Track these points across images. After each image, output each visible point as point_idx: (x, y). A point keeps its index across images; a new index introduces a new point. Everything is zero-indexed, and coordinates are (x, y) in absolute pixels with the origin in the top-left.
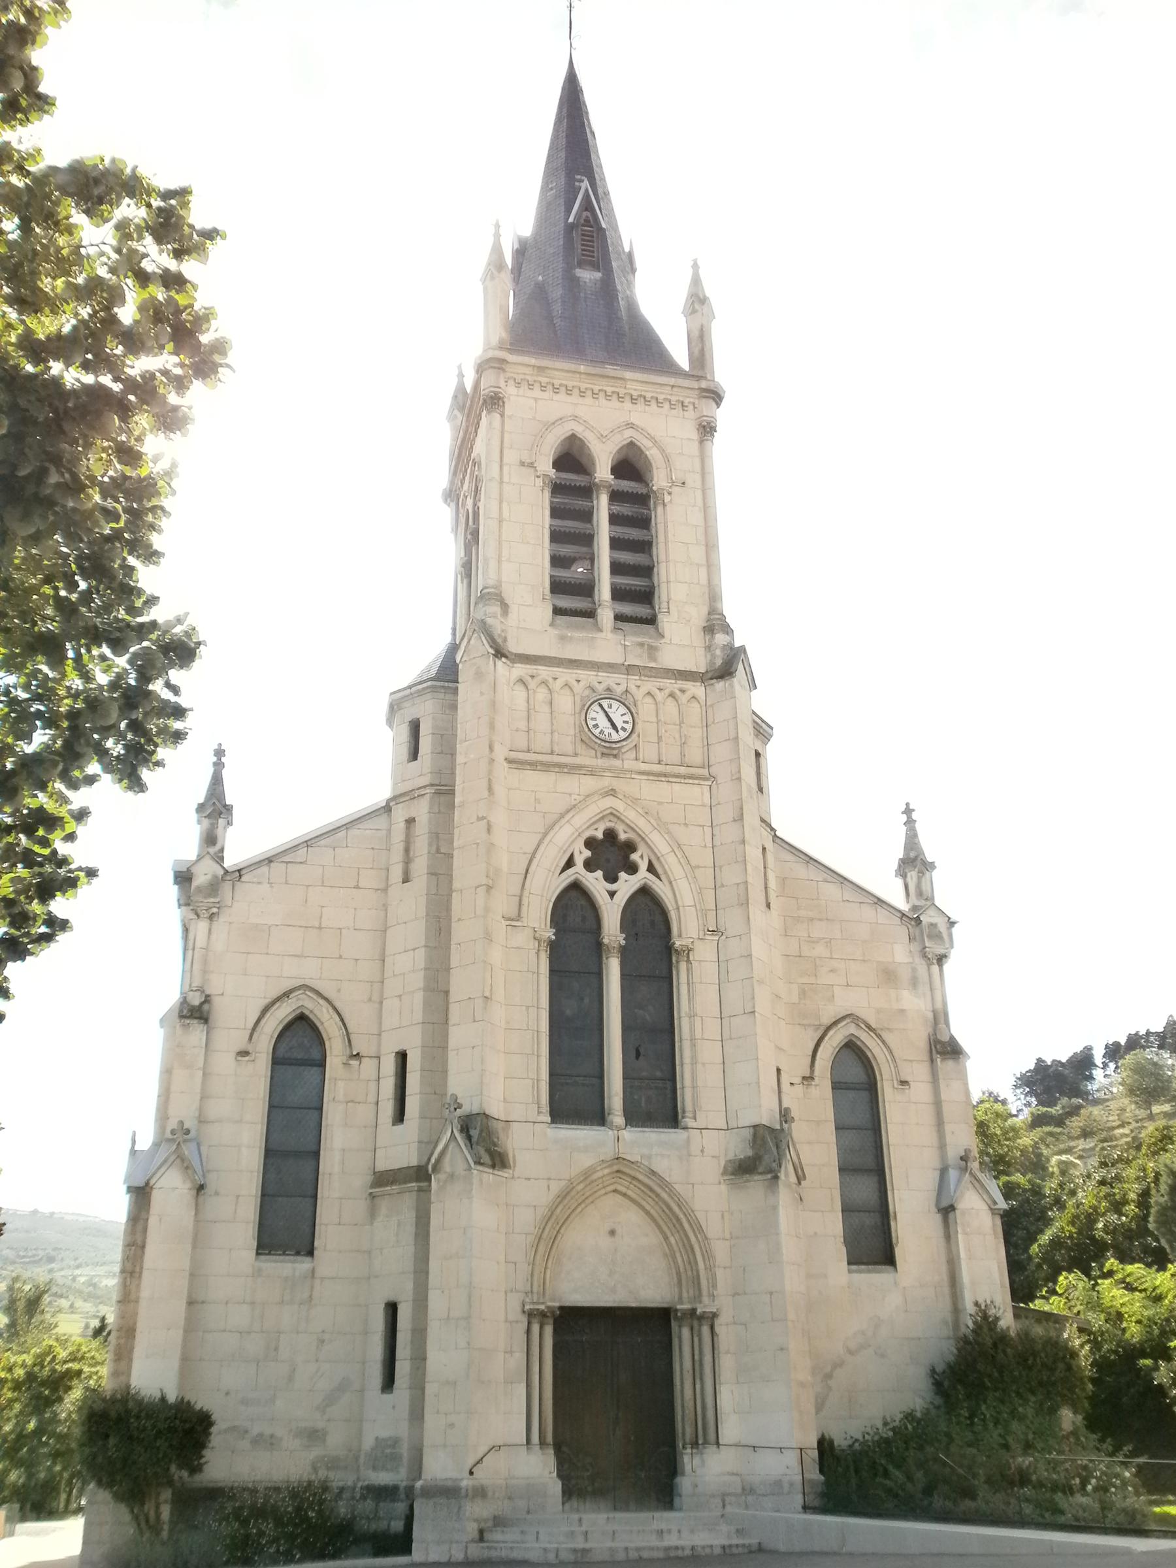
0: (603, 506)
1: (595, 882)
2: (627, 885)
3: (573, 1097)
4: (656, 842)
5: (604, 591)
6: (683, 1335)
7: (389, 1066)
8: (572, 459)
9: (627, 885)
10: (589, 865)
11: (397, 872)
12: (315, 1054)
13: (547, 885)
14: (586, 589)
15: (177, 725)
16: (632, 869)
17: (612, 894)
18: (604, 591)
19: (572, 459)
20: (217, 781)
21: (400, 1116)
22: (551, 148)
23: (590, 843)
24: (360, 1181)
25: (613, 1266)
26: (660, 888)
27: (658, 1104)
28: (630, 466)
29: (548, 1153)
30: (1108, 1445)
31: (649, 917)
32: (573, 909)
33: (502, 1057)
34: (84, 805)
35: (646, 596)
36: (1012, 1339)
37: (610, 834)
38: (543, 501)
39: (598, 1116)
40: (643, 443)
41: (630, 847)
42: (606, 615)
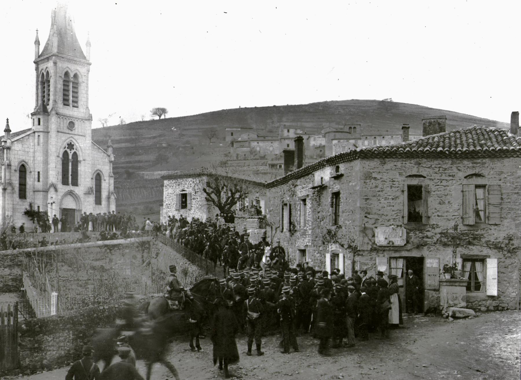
1: (68, 151)
2: (73, 151)
3: (65, 182)
4: (77, 145)
7: (37, 174)
8: (67, 74)
9: (73, 151)
10: (68, 148)
11: (36, 143)
12: (24, 170)
13: (62, 151)
14: (68, 100)
15: (72, 75)
16: (73, 149)
20: (8, 125)
22: (230, 110)
27: (75, 183)
28: (76, 76)
29: (63, 189)
31: (75, 154)
32: (66, 154)
33: (54, 175)
35: (76, 102)
37: (71, 143)
39: (68, 184)
40: (78, 73)
41: (73, 145)
42: (71, 105)
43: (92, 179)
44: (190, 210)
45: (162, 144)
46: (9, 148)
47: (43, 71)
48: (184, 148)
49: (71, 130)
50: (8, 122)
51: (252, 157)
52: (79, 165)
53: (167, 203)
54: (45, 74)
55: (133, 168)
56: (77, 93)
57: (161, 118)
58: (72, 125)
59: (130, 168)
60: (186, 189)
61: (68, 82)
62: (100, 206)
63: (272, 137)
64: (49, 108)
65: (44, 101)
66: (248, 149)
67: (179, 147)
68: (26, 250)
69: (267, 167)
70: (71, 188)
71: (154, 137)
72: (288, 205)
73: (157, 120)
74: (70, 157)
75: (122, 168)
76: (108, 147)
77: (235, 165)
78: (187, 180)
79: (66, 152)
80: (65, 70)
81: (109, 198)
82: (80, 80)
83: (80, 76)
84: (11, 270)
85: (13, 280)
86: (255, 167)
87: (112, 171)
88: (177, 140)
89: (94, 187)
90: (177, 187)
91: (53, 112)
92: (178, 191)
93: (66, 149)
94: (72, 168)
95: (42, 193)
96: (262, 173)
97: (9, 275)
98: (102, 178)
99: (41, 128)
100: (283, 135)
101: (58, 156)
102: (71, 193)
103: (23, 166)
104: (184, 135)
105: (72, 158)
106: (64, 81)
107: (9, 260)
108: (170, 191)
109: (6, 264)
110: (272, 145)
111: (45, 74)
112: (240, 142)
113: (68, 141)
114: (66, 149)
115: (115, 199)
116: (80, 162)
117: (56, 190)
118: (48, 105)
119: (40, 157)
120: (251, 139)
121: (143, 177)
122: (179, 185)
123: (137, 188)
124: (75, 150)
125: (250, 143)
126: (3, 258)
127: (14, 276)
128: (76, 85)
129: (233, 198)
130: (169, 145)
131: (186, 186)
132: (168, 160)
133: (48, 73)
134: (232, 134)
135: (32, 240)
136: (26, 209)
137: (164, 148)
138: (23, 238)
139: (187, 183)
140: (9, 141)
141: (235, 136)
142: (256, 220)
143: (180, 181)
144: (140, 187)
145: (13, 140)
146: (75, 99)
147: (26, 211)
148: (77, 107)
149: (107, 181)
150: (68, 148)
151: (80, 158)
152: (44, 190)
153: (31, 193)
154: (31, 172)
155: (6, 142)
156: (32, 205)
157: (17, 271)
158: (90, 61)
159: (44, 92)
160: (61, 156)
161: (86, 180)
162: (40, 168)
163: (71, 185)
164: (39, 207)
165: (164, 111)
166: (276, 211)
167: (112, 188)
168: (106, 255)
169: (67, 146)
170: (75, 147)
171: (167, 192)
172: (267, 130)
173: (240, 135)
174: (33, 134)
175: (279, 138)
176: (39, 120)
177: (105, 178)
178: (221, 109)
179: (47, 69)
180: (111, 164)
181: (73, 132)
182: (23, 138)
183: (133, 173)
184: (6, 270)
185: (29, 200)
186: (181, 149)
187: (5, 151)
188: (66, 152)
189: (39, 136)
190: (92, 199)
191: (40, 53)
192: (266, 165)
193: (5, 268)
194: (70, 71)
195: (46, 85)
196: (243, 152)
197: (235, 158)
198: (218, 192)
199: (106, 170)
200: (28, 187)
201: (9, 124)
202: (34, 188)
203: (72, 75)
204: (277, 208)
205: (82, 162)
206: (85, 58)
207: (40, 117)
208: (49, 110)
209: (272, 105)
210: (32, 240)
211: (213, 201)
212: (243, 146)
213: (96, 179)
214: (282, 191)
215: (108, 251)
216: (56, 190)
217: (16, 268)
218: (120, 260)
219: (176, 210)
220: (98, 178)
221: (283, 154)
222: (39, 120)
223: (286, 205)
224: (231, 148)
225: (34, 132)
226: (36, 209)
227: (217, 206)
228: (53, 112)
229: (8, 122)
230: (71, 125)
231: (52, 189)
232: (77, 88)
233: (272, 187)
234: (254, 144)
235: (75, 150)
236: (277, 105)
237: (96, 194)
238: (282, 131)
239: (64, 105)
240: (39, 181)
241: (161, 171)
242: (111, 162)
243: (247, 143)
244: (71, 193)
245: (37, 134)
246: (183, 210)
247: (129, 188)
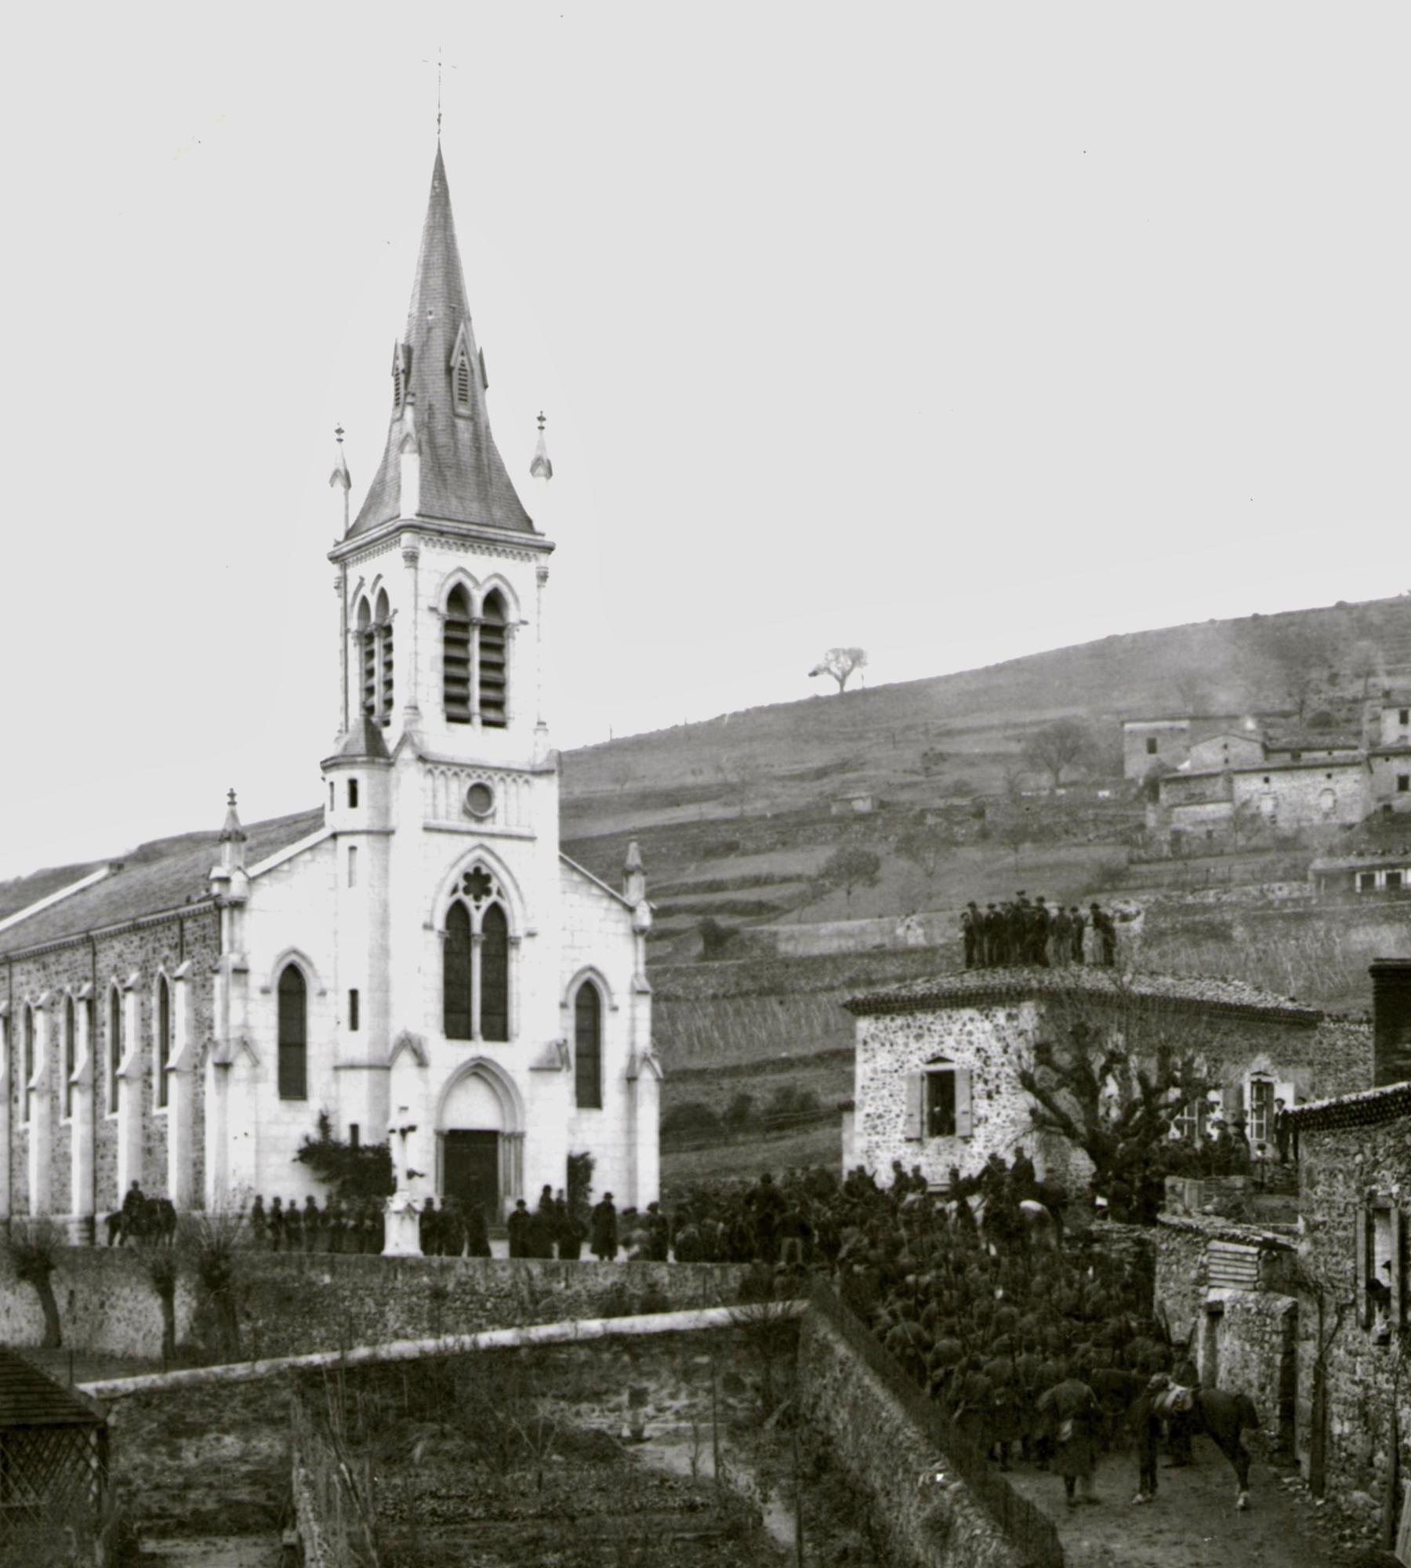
0: (475, 638)
1: (469, 901)
2: (486, 902)
3: (456, 1026)
4: (500, 878)
5: (475, 704)
6: (502, 1147)
9: (486, 902)
10: (466, 891)
13: (444, 903)
14: (463, 700)
15: (477, 598)
16: (488, 892)
17: (478, 908)
18: (475, 704)
19: (458, 597)
23: (467, 876)
25: (475, 1111)
26: (504, 904)
27: (498, 1029)
28: (494, 601)
30: (285, 1207)
31: (496, 915)
32: (458, 914)
33: (419, 1001)
34: (285, 946)
36: (502, 1212)
37: (477, 870)
38: (440, 665)
39: (467, 1036)
41: (487, 879)
42: (477, 720)
43: (563, 1006)
44: (967, 1139)
45: (850, 801)
46: (238, 905)
47: (365, 591)
48: (946, 813)
49: (480, 820)
50: (232, 803)
51: (1242, 842)
52: (513, 954)
53: (867, 1110)
54: (373, 602)
55: (732, 908)
56: (499, 667)
57: (848, 688)
58: (480, 797)
59: (721, 909)
60: (948, 1054)
61: (464, 626)
62: (594, 1114)
63: (1330, 749)
64: (390, 737)
65: (370, 710)
66: (1223, 810)
67: (923, 813)
68: (303, 1360)
69: (1309, 888)
70: (479, 1048)
71: (821, 773)
72: (1394, 1216)
73: (828, 700)
74: (477, 926)
75: (691, 910)
76: (628, 873)
77: (1167, 880)
78: (955, 1014)
80: (451, 583)
81: (631, 1079)
82: (512, 615)
84: (247, 1441)
85: (253, 1478)
86: (1253, 890)
87: (641, 968)
88: (915, 778)
89: (571, 1037)
90: (913, 1045)
91: (407, 754)
92: (917, 1063)
93: (460, 895)
94: (484, 1000)
95: (365, 1074)
96: (1286, 918)
97: (237, 1459)
98: (605, 1001)
99: (361, 817)
100: (1380, 735)
101: (428, 927)
102: (480, 1069)
104: (942, 757)
105: (485, 929)
106: (449, 625)
107: (236, 1402)
108: (884, 1059)
109: (228, 1416)
110: (1330, 784)
111: (373, 602)
112: (1187, 779)
113: (467, 865)
114: (460, 895)
115: (658, 1080)
116: (516, 943)
117: (422, 1062)
118: (387, 723)
120: (1234, 766)
121: (773, 948)
122: (919, 1037)
123: (745, 994)
124: (494, 897)
125: (1230, 781)
126: (215, 1396)
127: (257, 1463)
128: (495, 635)
129: (1152, 1112)
130: (883, 805)
131: (950, 1041)
132: (879, 874)
133: (383, 596)
134: (1152, 748)
135: (327, 1279)
136: (307, 1139)
137: (861, 817)
138: (295, 1272)
139: (956, 1028)
140: (238, 879)
141: (1163, 755)
142: (1254, 1250)
143: (925, 1019)
144: (762, 993)
145: (253, 871)
146: (492, 675)
147: (304, 1145)
148: (500, 725)
149: (625, 1011)
150: (466, 891)
152: (374, 1062)
153: (328, 1074)
154: (323, 993)
155: (226, 881)
156: (331, 1121)
157: (268, 1444)
158: (548, 539)
159: (370, 673)
160: (440, 923)
161: (539, 1014)
163: (478, 1037)
164: (354, 1129)
165: (857, 658)
166: (1340, 1233)
167: (644, 1040)
168: (621, 1377)
169: (462, 884)
170: (494, 885)
171: (868, 1067)
172: (1308, 715)
173: (1188, 749)
174: (329, 845)
175: (1363, 751)
176: (353, 784)
177: (617, 1001)
178: (1103, 636)
179: (381, 584)
180: (641, 941)
181: (486, 827)
182: (290, 860)
183: (733, 932)
184: (228, 1439)
185: (315, 1103)
186: (930, 820)
187: (225, 915)
190: (564, 1084)
191: (351, 524)
192: (1304, 879)
193: (226, 1432)
194: (469, 584)
195: (377, 645)
196: (1203, 822)
197: (1166, 850)
198: (1087, 1087)
199: (622, 966)
202: (336, 1055)
203: (477, 598)
204: (1346, 1220)
205: (525, 944)
206: (527, 524)
207: (358, 774)
208: (391, 746)
209: (1331, 603)
210: (327, 1279)
211: (1068, 1129)
212: (1200, 799)
213: (579, 1007)
214: (1368, 1152)
215: (626, 1358)
216: (422, 1062)
217: (266, 1431)
218: (673, 1396)
219: (909, 1140)
220: (588, 1001)
221: (1370, 981)
222: (353, 784)
223: (1384, 1212)
224: (1150, 807)
225: (334, 836)
226: (344, 1136)
227: (1083, 1145)
228: (407, 754)
229: (232, 803)
230: (481, 795)
231: (406, 1059)
232: (499, 648)
233: (1320, 1127)
234: (1248, 787)
235: (494, 897)
236: (1351, 599)
237: (579, 1067)
238: (1376, 719)
239: (451, 719)
240: (354, 1025)
241: (849, 918)
242: (638, 932)
243: (1221, 781)
244: (480, 1069)
245: (344, 842)
246: (937, 1140)
247: (715, 997)
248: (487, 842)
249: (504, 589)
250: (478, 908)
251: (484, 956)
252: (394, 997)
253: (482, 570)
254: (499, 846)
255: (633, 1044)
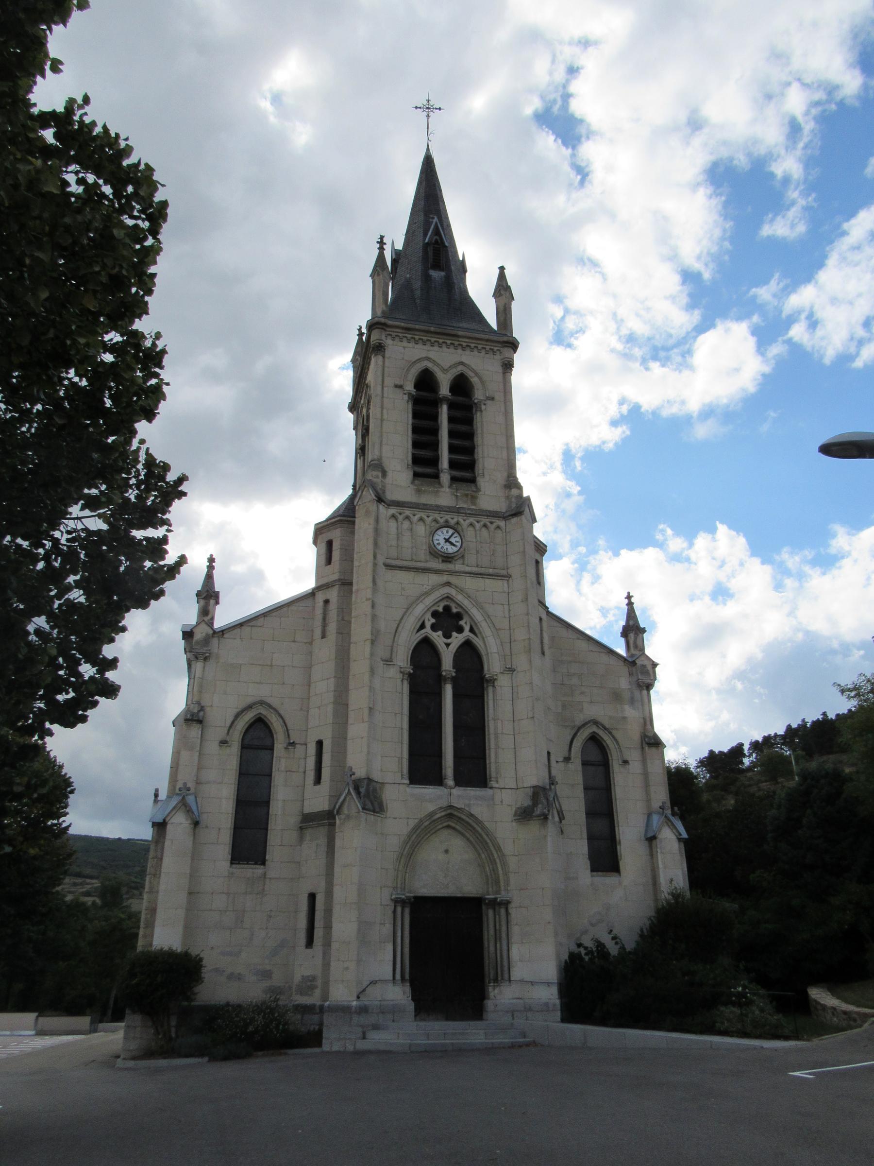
1: (437, 638)
2: (457, 639)
3: (423, 768)
7: (312, 749)
9: (457, 639)
10: (434, 628)
11: (318, 632)
13: (407, 640)
14: (434, 462)
17: (448, 645)
19: (426, 381)
21: (318, 780)
24: (294, 820)
25: (448, 870)
26: (477, 641)
27: (474, 770)
28: (462, 386)
31: (469, 655)
32: (424, 651)
33: (378, 743)
37: (447, 609)
39: (437, 780)
42: (445, 478)
62: (610, 880)
79: (426, 642)
83: (474, 380)
102: (452, 819)
103: (260, 722)
119: (324, 686)
132: (655, 366)
150: (434, 628)
151: (493, 665)
162: (319, 725)
169: (430, 621)
188: (426, 642)
189: (327, 602)
200: (277, 808)
201: (216, 573)
232: (470, 422)
244: (452, 819)
248: (453, 580)
249: (469, 374)
250: (448, 645)
251: (455, 695)
252: (153, 798)
253: (445, 361)
254: (469, 583)
255: (673, 257)
